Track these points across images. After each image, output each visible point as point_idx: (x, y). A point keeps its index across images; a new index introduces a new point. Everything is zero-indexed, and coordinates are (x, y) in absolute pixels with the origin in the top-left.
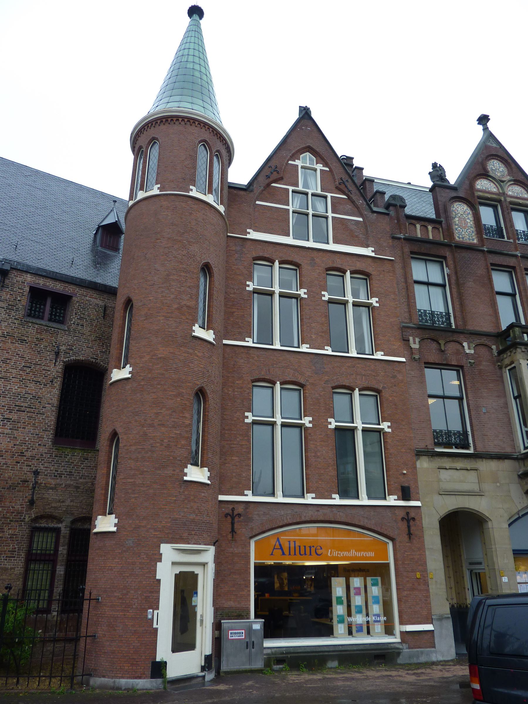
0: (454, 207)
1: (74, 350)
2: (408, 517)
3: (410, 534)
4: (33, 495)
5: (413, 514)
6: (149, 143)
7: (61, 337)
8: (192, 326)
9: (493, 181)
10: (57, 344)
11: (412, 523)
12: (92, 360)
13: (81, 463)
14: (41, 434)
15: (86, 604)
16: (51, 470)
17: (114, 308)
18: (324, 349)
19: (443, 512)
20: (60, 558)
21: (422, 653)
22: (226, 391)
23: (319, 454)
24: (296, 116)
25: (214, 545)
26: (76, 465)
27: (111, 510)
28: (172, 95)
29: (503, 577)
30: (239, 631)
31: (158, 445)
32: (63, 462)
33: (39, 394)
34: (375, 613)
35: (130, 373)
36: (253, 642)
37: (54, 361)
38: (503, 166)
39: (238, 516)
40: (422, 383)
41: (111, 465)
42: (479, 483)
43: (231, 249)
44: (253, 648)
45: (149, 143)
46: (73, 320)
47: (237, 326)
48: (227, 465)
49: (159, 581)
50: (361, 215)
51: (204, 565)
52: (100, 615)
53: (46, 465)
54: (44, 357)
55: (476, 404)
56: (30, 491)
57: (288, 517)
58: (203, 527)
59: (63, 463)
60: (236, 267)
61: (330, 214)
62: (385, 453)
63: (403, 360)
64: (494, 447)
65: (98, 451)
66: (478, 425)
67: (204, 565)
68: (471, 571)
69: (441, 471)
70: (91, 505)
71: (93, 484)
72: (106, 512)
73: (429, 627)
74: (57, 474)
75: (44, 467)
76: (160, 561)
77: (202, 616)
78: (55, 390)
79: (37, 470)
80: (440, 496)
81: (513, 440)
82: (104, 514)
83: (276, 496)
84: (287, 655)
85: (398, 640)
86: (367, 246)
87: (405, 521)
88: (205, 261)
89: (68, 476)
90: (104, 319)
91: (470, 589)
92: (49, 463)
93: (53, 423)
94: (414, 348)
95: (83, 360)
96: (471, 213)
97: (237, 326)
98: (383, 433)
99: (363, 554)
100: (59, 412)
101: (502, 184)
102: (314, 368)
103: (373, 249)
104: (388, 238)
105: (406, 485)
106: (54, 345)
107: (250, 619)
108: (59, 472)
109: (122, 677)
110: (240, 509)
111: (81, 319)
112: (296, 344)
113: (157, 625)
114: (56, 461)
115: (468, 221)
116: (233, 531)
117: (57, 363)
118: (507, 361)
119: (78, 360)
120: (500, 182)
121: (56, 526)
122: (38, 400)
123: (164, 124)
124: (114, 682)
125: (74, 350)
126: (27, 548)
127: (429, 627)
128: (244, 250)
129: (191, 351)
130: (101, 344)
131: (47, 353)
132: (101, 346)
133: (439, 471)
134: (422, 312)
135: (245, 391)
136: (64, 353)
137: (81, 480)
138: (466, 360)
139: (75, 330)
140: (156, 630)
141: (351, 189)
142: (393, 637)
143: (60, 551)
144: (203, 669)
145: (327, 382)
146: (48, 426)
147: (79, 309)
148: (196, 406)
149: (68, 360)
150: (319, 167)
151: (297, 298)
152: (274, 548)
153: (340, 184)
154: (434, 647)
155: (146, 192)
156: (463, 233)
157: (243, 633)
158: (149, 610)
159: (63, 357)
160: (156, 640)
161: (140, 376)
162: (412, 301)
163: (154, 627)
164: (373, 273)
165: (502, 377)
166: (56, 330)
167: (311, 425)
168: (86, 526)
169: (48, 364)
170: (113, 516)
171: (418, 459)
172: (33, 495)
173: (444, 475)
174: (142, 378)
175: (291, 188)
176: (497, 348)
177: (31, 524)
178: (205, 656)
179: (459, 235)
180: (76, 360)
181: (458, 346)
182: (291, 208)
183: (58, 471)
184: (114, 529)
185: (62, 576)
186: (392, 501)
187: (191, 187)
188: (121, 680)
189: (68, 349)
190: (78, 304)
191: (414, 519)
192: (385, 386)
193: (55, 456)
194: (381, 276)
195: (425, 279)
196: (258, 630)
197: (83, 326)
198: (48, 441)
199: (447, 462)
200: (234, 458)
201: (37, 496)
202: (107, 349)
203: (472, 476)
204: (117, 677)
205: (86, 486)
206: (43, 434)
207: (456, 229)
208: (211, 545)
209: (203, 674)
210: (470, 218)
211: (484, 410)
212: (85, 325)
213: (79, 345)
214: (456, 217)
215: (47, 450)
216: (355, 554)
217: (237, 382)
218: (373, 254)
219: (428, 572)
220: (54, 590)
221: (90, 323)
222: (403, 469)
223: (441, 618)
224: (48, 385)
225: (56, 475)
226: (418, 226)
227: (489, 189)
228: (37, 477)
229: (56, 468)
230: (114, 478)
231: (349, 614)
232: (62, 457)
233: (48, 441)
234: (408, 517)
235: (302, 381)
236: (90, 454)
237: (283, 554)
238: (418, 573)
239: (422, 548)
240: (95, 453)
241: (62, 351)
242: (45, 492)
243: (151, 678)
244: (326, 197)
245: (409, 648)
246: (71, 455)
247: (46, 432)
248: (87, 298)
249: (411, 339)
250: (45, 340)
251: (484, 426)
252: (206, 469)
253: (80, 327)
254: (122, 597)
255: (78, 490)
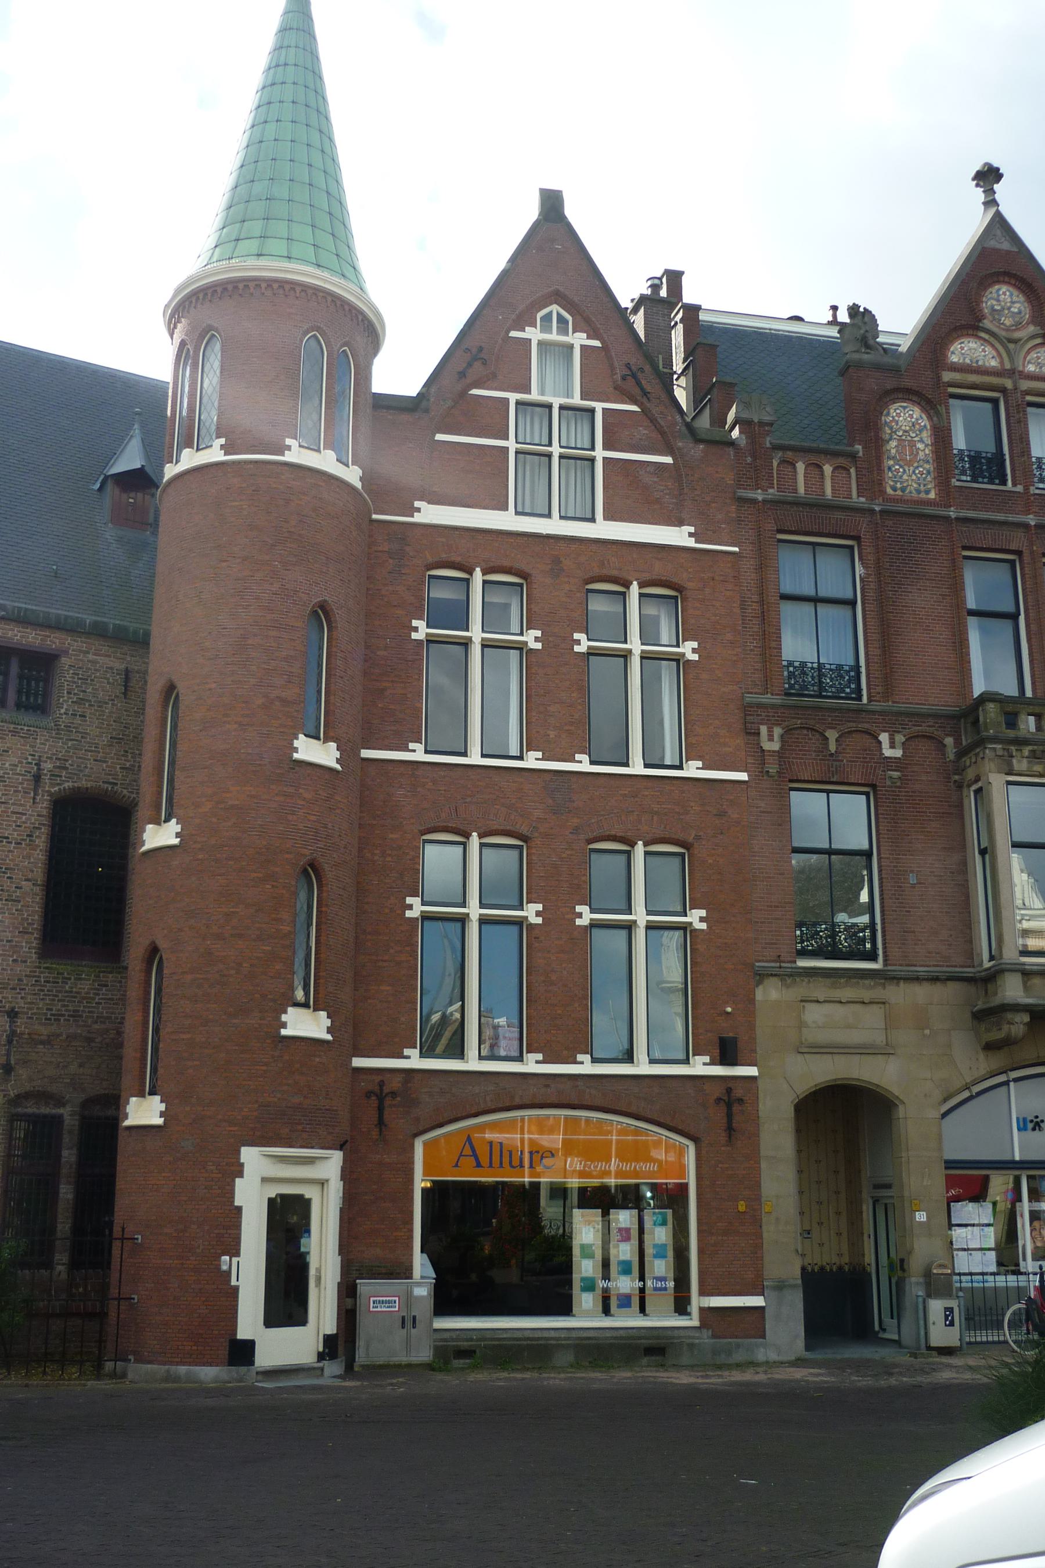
0: (888, 414)
1: (70, 767)
2: (729, 1097)
3: (730, 1129)
4: (8, 1055)
5: (741, 1091)
6: (202, 337)
7: (42, 744)
8: (292, 740)
9: (992, 340)
10: (36, 757)
11: (736, 1108)
12: (106, 786)
13: (94, 994)
14: (17, 939)
15: (116, 1245)
16: (38, 1008)
17: (146, 672)
18: (573, 760)
19: (804, 1087)
20: (64, 1171)
21: (738, 1346)
22: (368, 855)
23: (554, 978)
24: (531, 213)
25: (341, 1150)
26: (84, 998)
27: (154, 1087)
28: (241, 237)
29: (917, 1213)
30: (388, 1299)
31: (233, 972)
32: (60, 992)
33: (8, 861)
34: (657, 1274)
35: (178, 835)
36: (414, 1318)
37: (32, 795)
38: (1022, 298)
39: (390, 1095)
40: (780, 825)
41: (150, 1006)
42: (886, 1029)
43: (380, 549)
44: (414, 1327)
45: (202, 337)
46: (65, 707)
47: (392, 720)
48: (369, 1001)
49: (239, 1209)
50: (669, 451)
51: (323, 1184)
52: (141, 1265)
53: (29, 998)
54: (12, 787)
55: (896, 867)
56: (4, 1048)
57: (488, 1098)
58: (317, 1117)
59: (60, 995)
60: (390, 588)
61: (600, 453)
62: (691, 972)
63: (743, 776)
64: (926, 956)
65: (126, 968)
66: (896, 911)
67: (323, 1183)
68: (876, 1201)
69: (808, 1005)
70: (117, 1073)
71: (119, 1033)
72: (144, 1090)
73: (757, 1301)
74: (51, 1015)
75: (25, 1003)
76: (240, 1174)
77: (319, 1270)
78: (38, 852)
79: (13, 1009)
80: (800, 1057)
81: (971, 942)
82: (141, 1094)
83: (466, 1058)
84: (479, 1343)
85: (695, 1323)
86: (680, 523)
87: (722, 1104)
88: (318, 600)
89: (71, 1019)
90: (125, 698)
91: (871, 1236)
92: (35, 994)
93: (36, 917)
94: (769, 751)
95: (87, 788)
96: (929, 427)
97: (392, 720)
98: (691, 931)
99: (635, 1167)
100: (47, 895)
101: (1011, 346)
102: (550, 801)
103: (692, 529)
104: (728, 501)
105: (731, 1035)
106: (30, 761)
107: (412, 1279)
108: (54, 1012)
109: (183, 1364)
110: (395, 1084)
111: (80, 702)
112: (514, 751)
113: (238, 1280)
114: (48, 991)
115: (920, 446)
116: (381, 1123)
117: (38, 798)
118: (970, 774)
119: (79, 788)
120: (1007, 343)
121: (54, 1111)
122: (6, 873)
123: (230, 296)
124: (168, 1371)
125: (70, 767)
126: (4, 1152)
127: (757, 1301)
128: (408, 549)
129: (291, 790)
130: (122, 753)
131: (18, 779)
132: (123, 755)
133: (804, 1006)
134: (795, 667)
135: (408, 854)
136: (51, 775)
137: (96, 1026)
138: (883, 771)
139: (70, 727)
140: (236, 1289)
141: (648, 389)
142: (689, 1317)
143: (65, 1158)
144: (321, 1356)
145: (576, 830)
146: (28, 924)
147: (75, 682)
148: (303, 895)
149: (60, 789)
150: (579, 339)
151: (521, 649)
152: (461, 1155)
153: (624, 378)
154: (763, 1336)
155: (198, 450)
156: (905, 477)
157: (395, 1302)
158: (223, 1258)
159: (50, 787)
160: (237, 1305)
161: (195, 842)
162: (773, 644)
163: (232, 1284)
164: (690, 585)
165: (960, 806)
166: (32, 729)
167: (539, 920)
168: (110, 1113)
169: (21, 800)
170: (158, 1098)
171: (759, 983)
172: (8, 1055)
173: (814, 1014)
174: (199, 846)
175: (513, 397)
176: (957, 742)
177: (8, 1108)
178: (324, 1335)
179: (896, 482)
180: (73, 789)
181: (867, 740)
182: (511, 445)
183: (51, 1010)
184: (160, 1121)
185: (71, 1202)
186: (700, 1067)
187: (288, 441)
188: (179, 1367)
189: (59, 767)
190: (71, 672)
191: (740, 1101)
192: (701, 833)
193: (44, 982)
194: (707, 591)
195: (808, 590)
196: (423, 1297)
197: (85, 716)
198: (31, 953)
199: (820, 990)
200: (382, 988)
201: (17, 1057)
202: (134, 761)
203: (873, 1016)
204: (171, 1363)
205: (105, 1036)
206: (20, 939)
207: (890, 469)
208: (336, 1149)
209: (320, 1365)
210: (925, 439)
211: (913, 880)
212: (88, 715)
213: (80, 758)
214: (890, 439)
215: (28, 970)
216: (619, 1165)
217: (391, 836)
218: (691, 543)
219: (763, 1199)
220: (57, 1227)
221: (97, 711)
222: (726, 1003)
223: (780, 1286)
224: (23, 843)
225: (49, 1016)
226: (800, 467)
227: (980, 363)
228: (14, 1022)
229: (47, 1004)
230: (156, 1030)
231: (606, 1276)
232: (58, 983)
233: (31, 953)
234: (729, 1097)
235: (524, 830)
236: (111, 975)
237: (479, 1165)
238: (742, 1202)
239: (754, 1156)
240: (119, 973)
241: (45, 772)
242: (30, 1050)
243: (229, 1366)
244: (592, 411)
245: (714, 1336)
246: (75, 979)
247: (26, 936)
248: (91, 657)
249: (764, 729)
250: (12, 752)
251: (909, 912)
252: (323, 1014)
253: (78, 721)
254: (176, 1235)
255: (93, 1044)
